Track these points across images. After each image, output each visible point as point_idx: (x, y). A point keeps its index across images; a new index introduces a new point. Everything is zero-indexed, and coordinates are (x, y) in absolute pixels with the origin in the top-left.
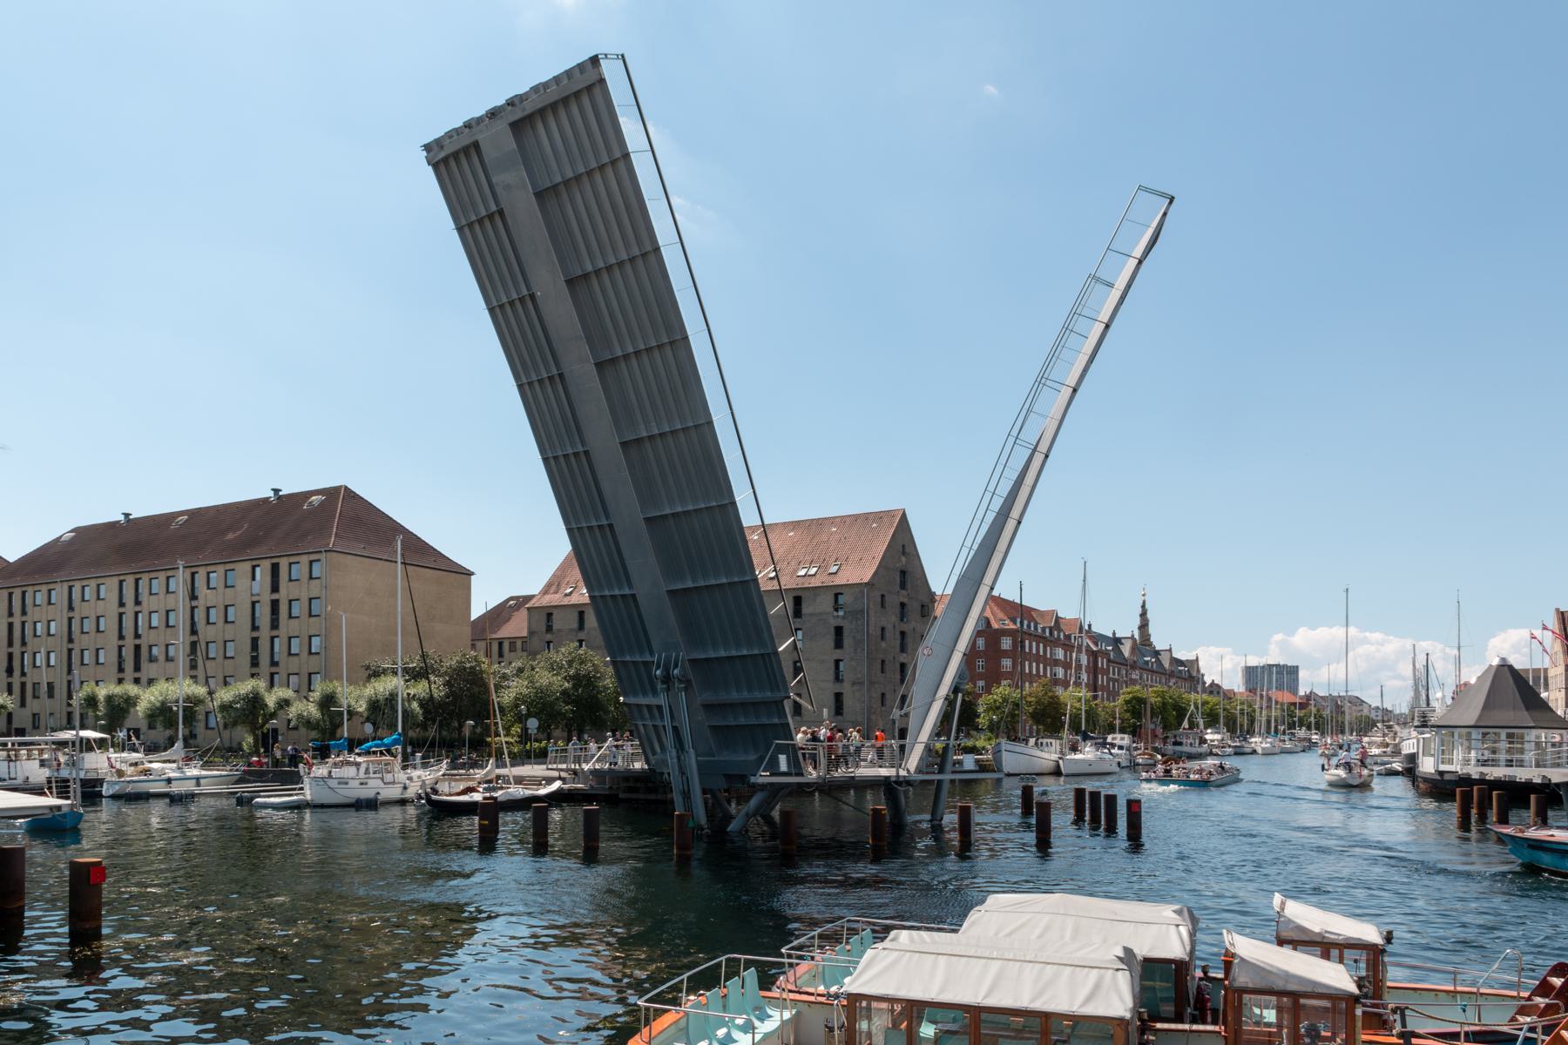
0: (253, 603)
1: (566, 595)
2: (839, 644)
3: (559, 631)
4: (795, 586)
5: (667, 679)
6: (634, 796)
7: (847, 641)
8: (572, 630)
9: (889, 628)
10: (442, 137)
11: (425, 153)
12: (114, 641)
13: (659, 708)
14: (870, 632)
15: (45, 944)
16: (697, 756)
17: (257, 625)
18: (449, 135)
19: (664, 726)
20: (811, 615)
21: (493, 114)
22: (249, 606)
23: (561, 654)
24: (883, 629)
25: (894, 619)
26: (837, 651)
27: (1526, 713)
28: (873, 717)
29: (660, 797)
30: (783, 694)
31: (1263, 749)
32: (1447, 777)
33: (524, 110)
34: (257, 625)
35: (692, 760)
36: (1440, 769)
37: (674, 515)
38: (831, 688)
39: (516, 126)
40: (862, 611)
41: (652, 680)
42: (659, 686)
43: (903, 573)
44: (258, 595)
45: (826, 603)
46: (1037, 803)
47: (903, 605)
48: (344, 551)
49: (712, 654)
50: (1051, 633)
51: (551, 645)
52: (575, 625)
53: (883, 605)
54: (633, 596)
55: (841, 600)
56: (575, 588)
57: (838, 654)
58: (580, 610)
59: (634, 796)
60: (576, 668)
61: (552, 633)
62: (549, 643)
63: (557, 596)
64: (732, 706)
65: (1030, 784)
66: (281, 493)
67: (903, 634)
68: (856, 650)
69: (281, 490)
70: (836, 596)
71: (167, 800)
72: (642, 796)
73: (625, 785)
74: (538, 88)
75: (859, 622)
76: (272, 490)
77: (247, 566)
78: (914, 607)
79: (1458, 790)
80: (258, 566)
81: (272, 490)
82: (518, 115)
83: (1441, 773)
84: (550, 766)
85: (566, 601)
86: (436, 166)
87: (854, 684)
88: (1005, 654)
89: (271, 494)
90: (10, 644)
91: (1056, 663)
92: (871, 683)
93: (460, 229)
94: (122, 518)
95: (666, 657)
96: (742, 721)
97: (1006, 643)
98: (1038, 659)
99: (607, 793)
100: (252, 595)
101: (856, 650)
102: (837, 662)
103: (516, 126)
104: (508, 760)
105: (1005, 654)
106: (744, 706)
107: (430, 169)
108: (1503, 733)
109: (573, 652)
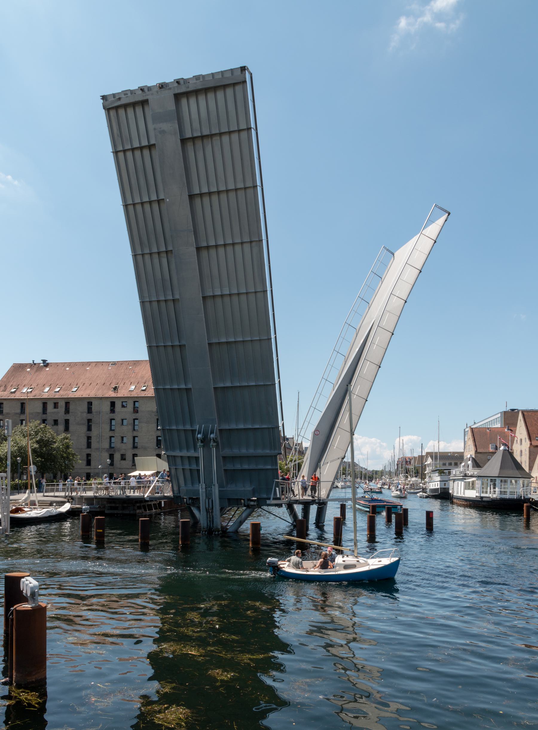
1: (12, 393)
3: (8, 414)
5: (205, 441)
6: (116, 512)
8: (17, 414)
10: (154, 86)
11: (102, 101)
13: (197, 459)
16: (219, 488)
18: (125, 93)
19: (198, 471)
21: (162, 86)
23: (32, 425)
27: (517, 471)
29: (132, 512)
30: (277, 452)
31: (342, 486)
32: (484, 499)
33: (188, 87)
35: (216, 491)
36: (481, 496)
37: (227, 343)
39: (177, 97)
41: (195, 440)
42: (199, 444)
48: (361, 323)
49: (233, 426)
51: (24, 422)
52: (19, 411)
54: (188, 390)
56: (18, 389)
58: (55, 402)
59: (116, 512)
60: (41, 436)
61: (3, 415)
62: (22, 421)
63: (6, 393)
64: (241, 458)
65: (344, 503)
70: (134, 402)
71: (338, 515)
72: (120, 512)
73: (109, 505)
74: (199, 78)
79: (525, 505)
82: (183, 89)
83: (482, 498)
84: (46, 494)
85: (12, 396)
86: (108, 110)
93: (116, 153)
95: (205, 427)
96: (246, 467)
99: (98, 510)
103: (177, 97)
104: (35, 489)
106: (249, 458)
107: (103, 112)
108: (489, 479)
109: (37, 427)
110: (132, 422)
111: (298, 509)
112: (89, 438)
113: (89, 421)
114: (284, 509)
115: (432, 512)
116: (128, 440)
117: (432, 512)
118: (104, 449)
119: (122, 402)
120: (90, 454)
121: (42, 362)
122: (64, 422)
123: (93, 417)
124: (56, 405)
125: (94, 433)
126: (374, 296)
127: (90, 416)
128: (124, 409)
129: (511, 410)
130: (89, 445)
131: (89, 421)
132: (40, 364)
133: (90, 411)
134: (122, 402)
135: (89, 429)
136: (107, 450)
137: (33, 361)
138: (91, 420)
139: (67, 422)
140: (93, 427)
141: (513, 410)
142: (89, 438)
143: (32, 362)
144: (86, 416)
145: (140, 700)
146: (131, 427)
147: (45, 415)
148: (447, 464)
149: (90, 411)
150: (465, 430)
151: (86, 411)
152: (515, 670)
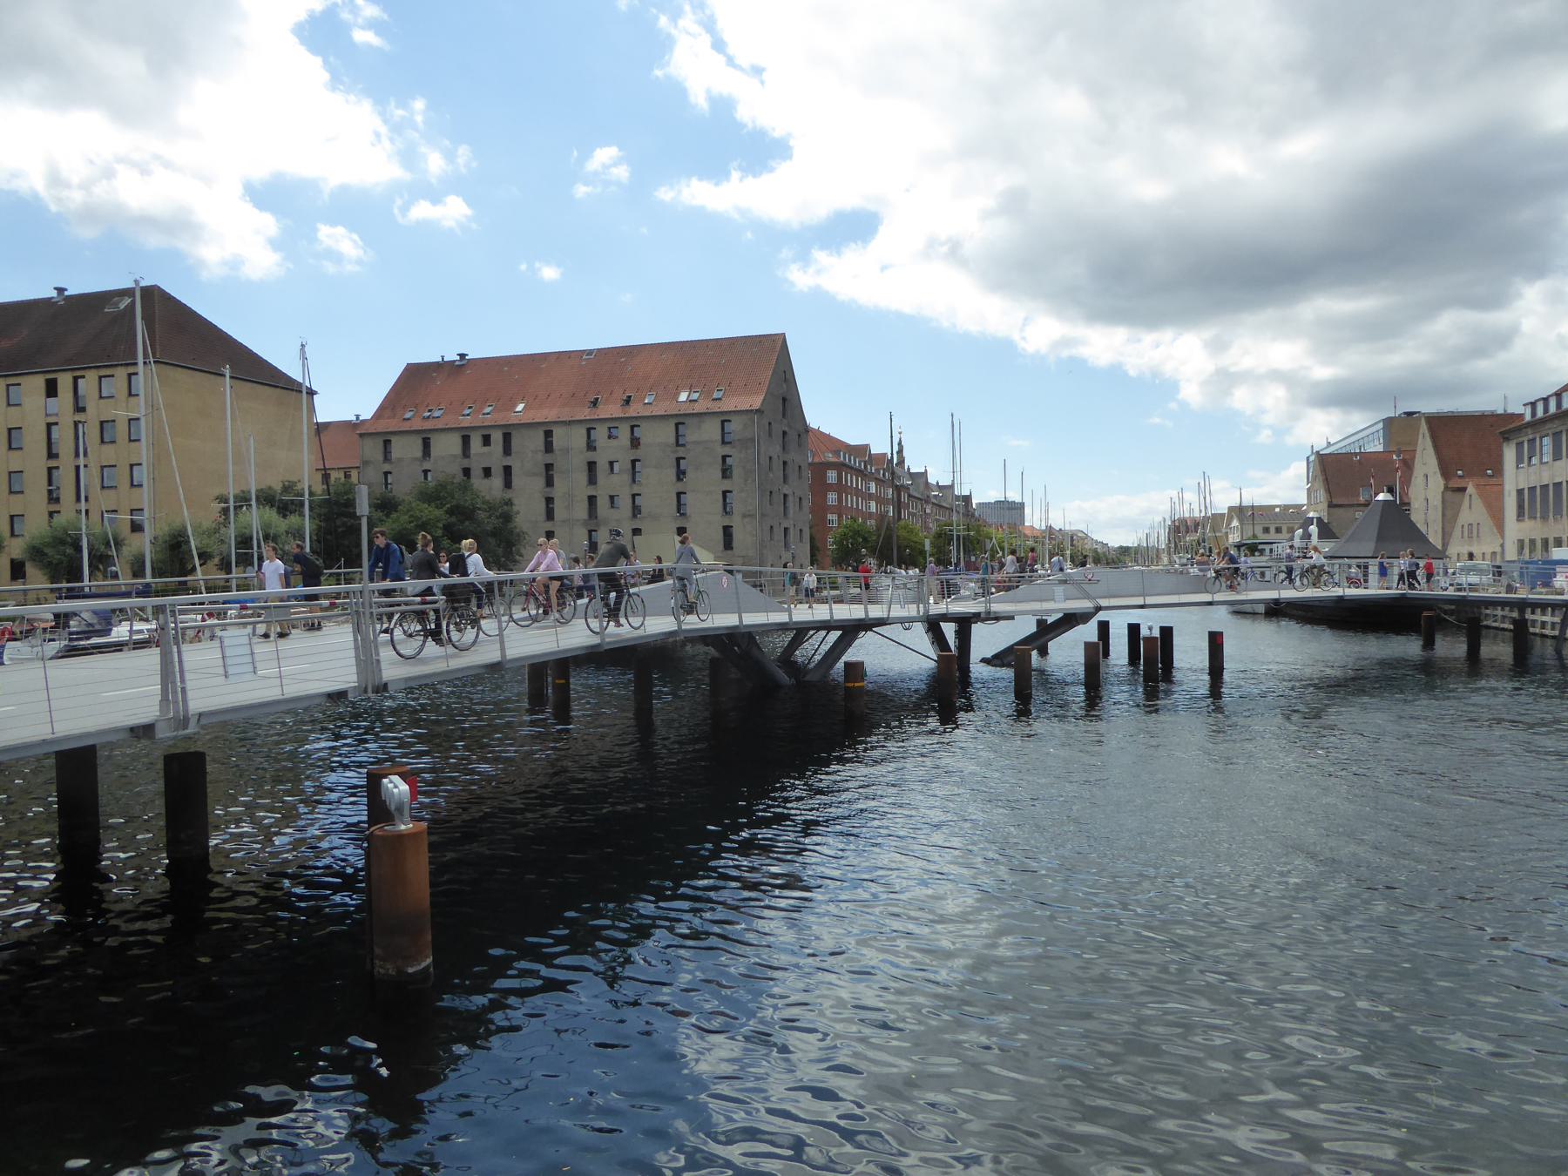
0: (49, 426)
2: (726, 473)
3: (400, 460)
4: (663, 413)
7: (736, 472)
8: (416, 459)
9: (775, 457)
12: (40, 462)
14: (761, 462)
15: (1556, 1108)
17: (54, 452)
20: (697, 443)
22: (44, 428)
24: (770, 458)
25: (778, 448)
26: (726, 481)
28: (765, 552)
34: (54, 452)
38: (719, 521)
40: (753, 440)
43: (784, 400)
44: (57, 415)
45: (711, 430)
46: (1146, 639)
47: (784, 433)
50: (865, 466)
52: (419, 454)
53: (770, 435)
55: (729, 427)
57: (727, 485)
66: (66, 293)
67: (785, 463)
68: (746, 481)
69: (66, 290)
75: (749, 451)
76: (55, 288)
77: (38, 382)
78: (792, 435)
80: (83, 377)
81: (55, 288)
87: (744, 516)
88: (830, 487)
89: (54, 294)
90: (77, 455)
91: (871, 497)
92: (763, 515)
94: (54, 294)
97: (832, 476)
98: (858, 492)
100: (47, 415)
101: (746, 481)
102: (725, 493)
105: (830, 487)
110: (630, 466)
111: (949, 630)
112: (549, 500)
113: (549, 467)
114: (919, 629)
115: (1221, 634)
116: (625, 503)
117: (1221, 634)
118: (578, 520)
119: (610, 428)
120: (553, 532)
121: (458, 358)
122: (501, 471)
123: (556, 459)
124: (487, 440)
125: (558, 491)
126: (176, 655)
127: (549, 459)
128: (613, 442)
129: (1405, 413)
130: (550, 515)
131: (549, 467)
132: (455, 361)
133: (549, 447)
134: (610, 428)
135: (549, 482)
136: (585, 523)
137: (443, 357)
138: (552, 465)
139: (507, 470)
140: (555, 479)
141: (1409, 414)
142: (549, 500)
143: (354, 418)
144: (542, 458)
145: (964, 971)
146: (627, 477)
147: (466, 461)
148: (1272, 530)
149: (549, 447)
150: (1308, 458)
151: (542, 448)
152: (986, 952)
